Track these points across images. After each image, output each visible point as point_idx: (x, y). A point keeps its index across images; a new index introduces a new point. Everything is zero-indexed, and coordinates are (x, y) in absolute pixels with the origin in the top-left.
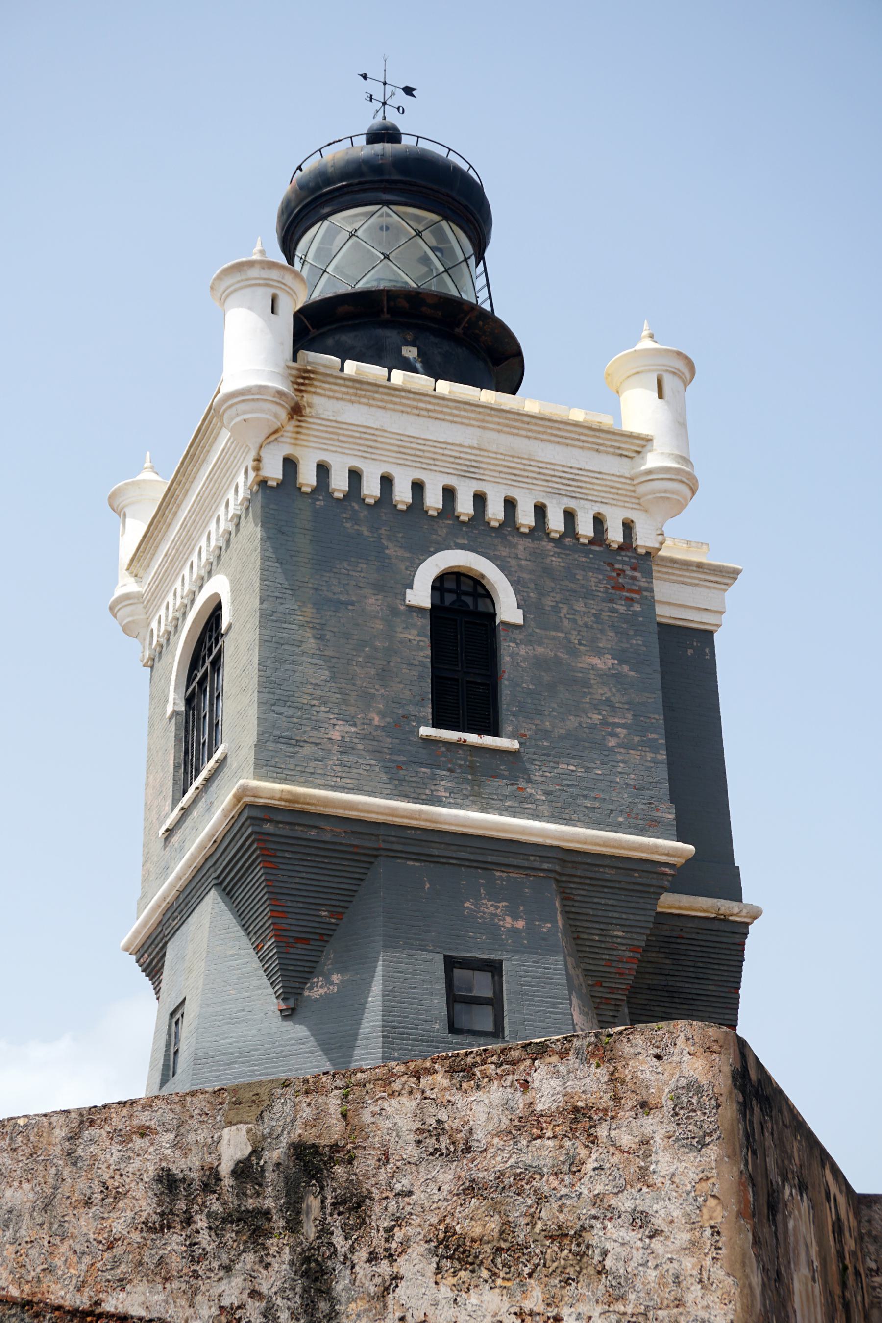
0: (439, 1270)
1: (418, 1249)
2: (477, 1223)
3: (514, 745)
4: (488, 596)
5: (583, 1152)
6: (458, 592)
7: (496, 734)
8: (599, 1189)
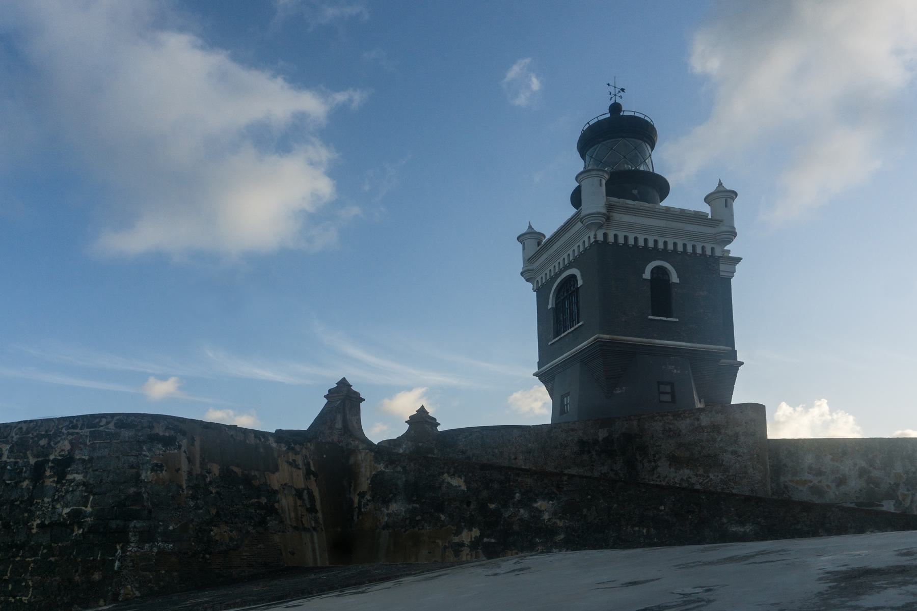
4: (652, 270)
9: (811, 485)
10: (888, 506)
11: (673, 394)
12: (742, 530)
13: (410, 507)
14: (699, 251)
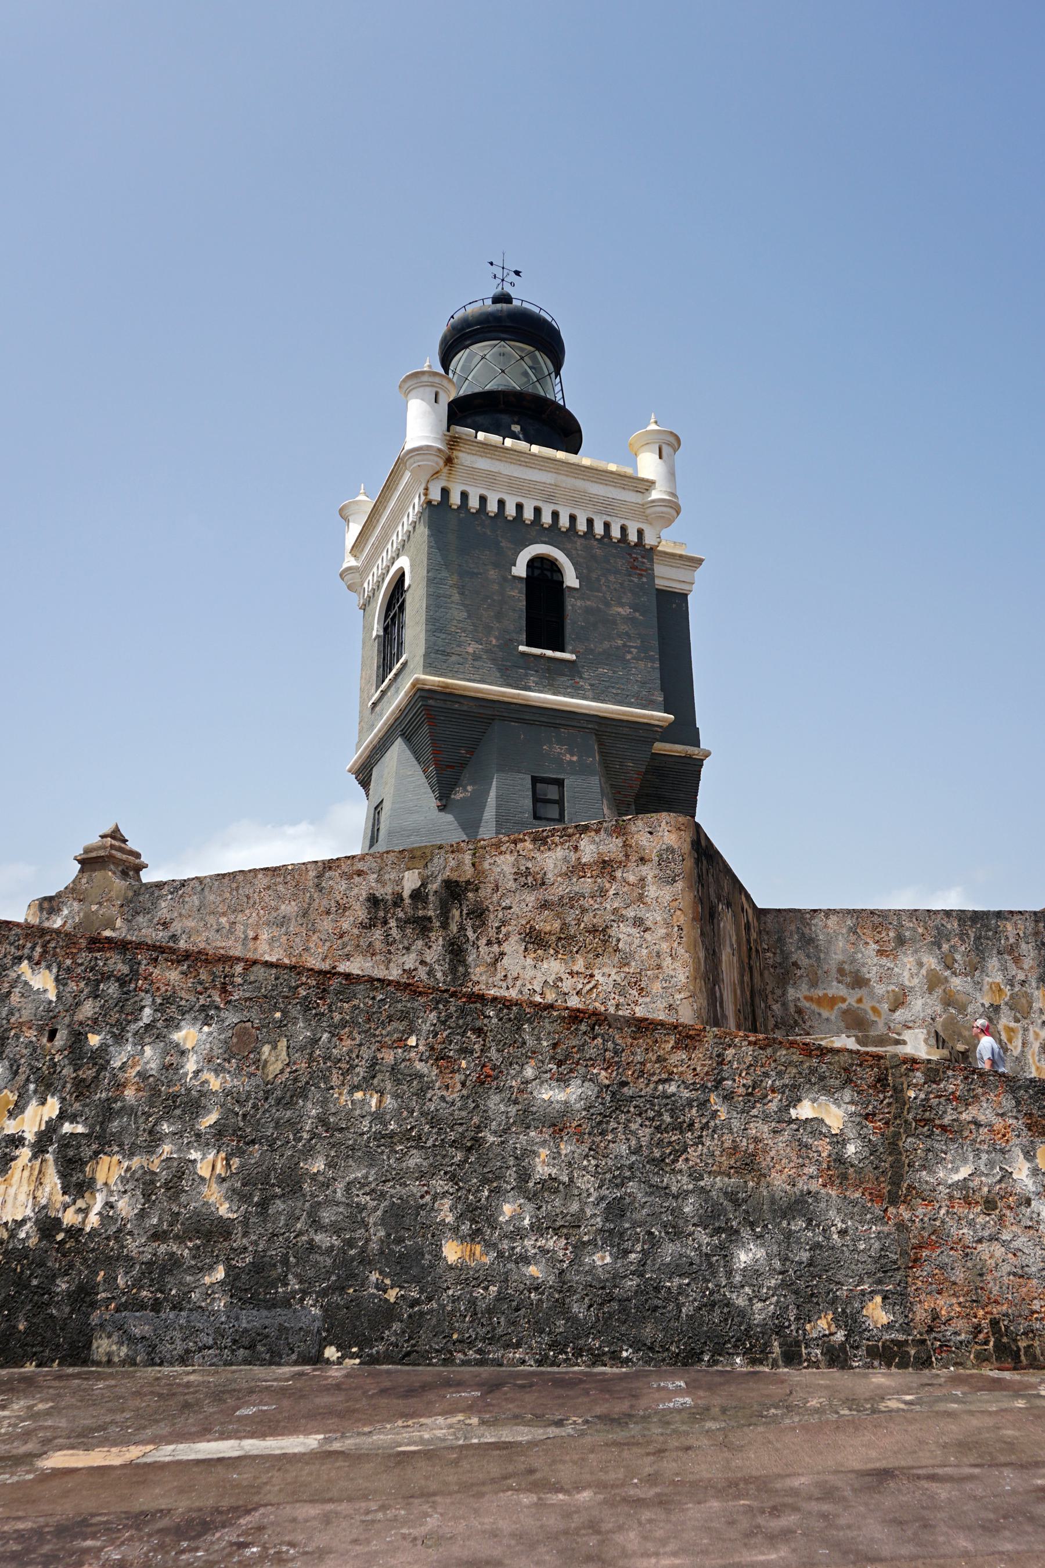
1: (514, 938)
2: (547, 923)
5: (608, 885)
7: (563, 651)
8: (616, 905)
9: (844, 1006)
12: (561, 1096)
14: (616, 533)
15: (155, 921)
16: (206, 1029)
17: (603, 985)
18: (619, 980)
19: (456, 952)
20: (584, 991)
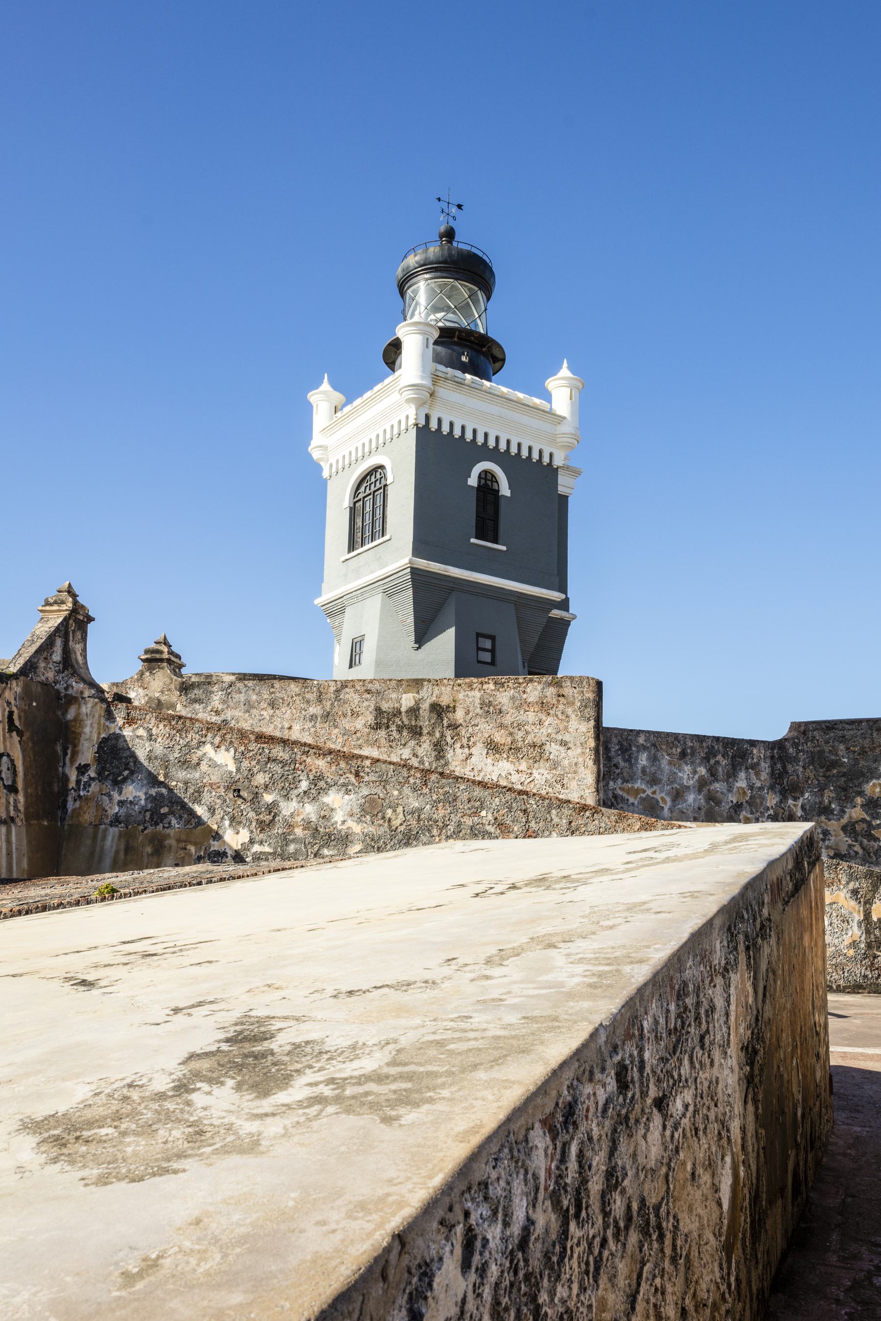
0: (487, 753)
1: (480, 745)
2: (500, 737)
3: (504, 548)
5: (544, 718)
6: (486, 479)
7: (497, 543)
8: (550, 731)
9: (644, 795)
10: (250, 684)
11: (493, 651)
13: (153, 792)
15: (209, 708)
16: (347, 797)
17: (540, 778)
18: (549, 778)
19: (439, 749)
20: (526, 783)
